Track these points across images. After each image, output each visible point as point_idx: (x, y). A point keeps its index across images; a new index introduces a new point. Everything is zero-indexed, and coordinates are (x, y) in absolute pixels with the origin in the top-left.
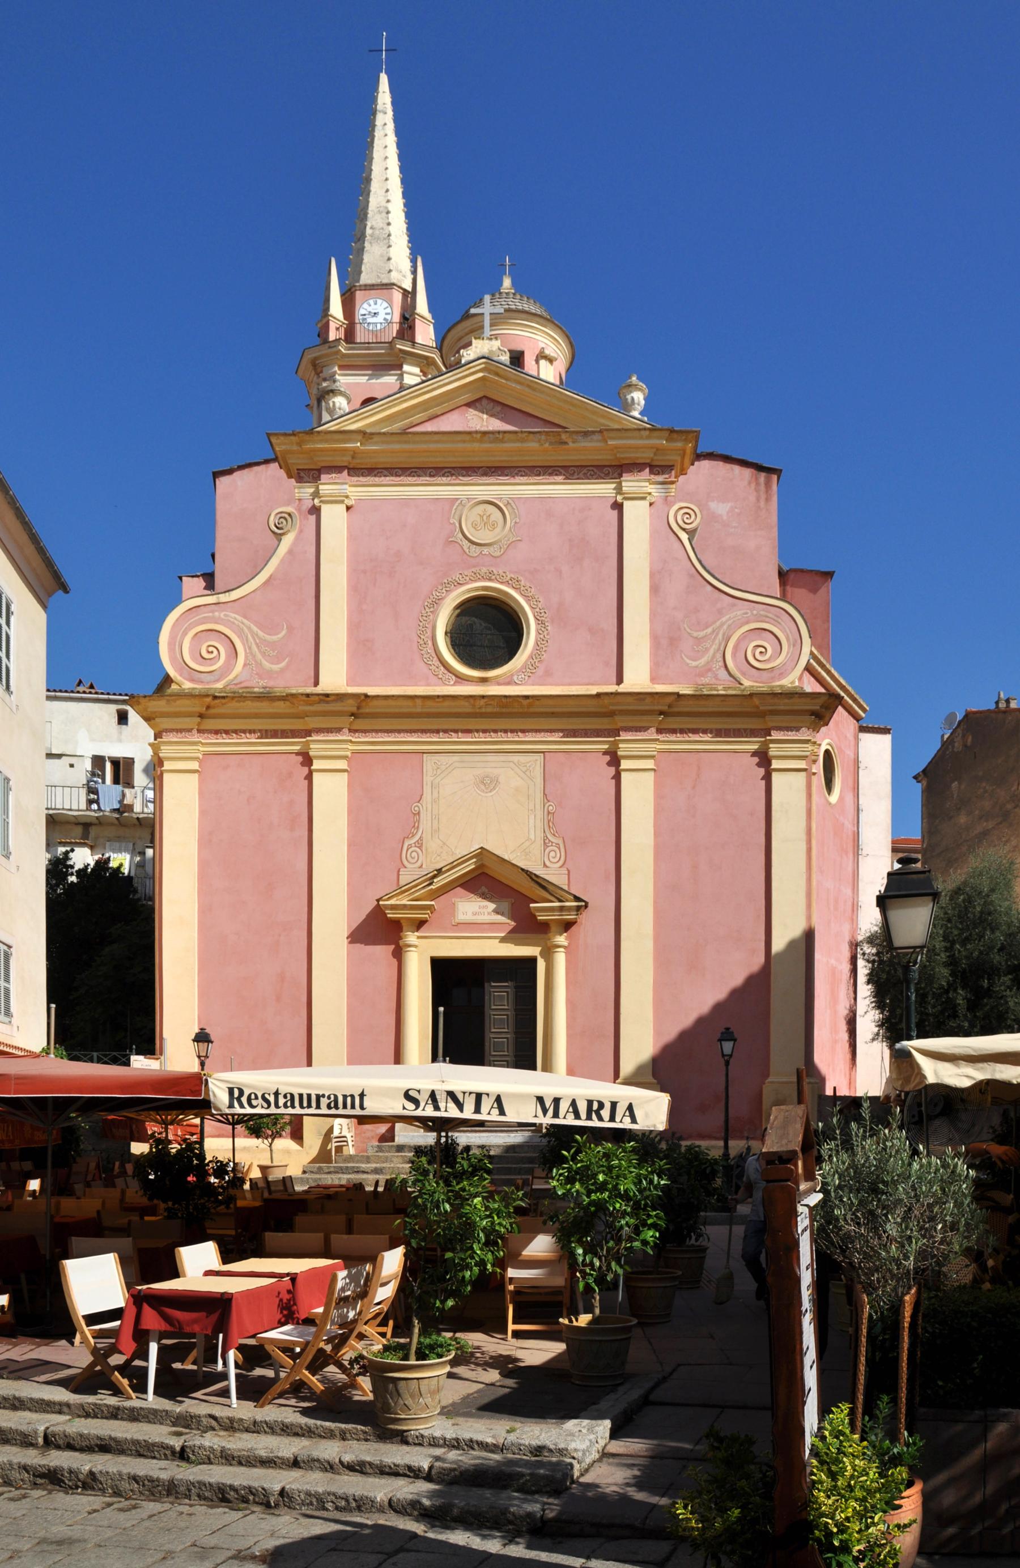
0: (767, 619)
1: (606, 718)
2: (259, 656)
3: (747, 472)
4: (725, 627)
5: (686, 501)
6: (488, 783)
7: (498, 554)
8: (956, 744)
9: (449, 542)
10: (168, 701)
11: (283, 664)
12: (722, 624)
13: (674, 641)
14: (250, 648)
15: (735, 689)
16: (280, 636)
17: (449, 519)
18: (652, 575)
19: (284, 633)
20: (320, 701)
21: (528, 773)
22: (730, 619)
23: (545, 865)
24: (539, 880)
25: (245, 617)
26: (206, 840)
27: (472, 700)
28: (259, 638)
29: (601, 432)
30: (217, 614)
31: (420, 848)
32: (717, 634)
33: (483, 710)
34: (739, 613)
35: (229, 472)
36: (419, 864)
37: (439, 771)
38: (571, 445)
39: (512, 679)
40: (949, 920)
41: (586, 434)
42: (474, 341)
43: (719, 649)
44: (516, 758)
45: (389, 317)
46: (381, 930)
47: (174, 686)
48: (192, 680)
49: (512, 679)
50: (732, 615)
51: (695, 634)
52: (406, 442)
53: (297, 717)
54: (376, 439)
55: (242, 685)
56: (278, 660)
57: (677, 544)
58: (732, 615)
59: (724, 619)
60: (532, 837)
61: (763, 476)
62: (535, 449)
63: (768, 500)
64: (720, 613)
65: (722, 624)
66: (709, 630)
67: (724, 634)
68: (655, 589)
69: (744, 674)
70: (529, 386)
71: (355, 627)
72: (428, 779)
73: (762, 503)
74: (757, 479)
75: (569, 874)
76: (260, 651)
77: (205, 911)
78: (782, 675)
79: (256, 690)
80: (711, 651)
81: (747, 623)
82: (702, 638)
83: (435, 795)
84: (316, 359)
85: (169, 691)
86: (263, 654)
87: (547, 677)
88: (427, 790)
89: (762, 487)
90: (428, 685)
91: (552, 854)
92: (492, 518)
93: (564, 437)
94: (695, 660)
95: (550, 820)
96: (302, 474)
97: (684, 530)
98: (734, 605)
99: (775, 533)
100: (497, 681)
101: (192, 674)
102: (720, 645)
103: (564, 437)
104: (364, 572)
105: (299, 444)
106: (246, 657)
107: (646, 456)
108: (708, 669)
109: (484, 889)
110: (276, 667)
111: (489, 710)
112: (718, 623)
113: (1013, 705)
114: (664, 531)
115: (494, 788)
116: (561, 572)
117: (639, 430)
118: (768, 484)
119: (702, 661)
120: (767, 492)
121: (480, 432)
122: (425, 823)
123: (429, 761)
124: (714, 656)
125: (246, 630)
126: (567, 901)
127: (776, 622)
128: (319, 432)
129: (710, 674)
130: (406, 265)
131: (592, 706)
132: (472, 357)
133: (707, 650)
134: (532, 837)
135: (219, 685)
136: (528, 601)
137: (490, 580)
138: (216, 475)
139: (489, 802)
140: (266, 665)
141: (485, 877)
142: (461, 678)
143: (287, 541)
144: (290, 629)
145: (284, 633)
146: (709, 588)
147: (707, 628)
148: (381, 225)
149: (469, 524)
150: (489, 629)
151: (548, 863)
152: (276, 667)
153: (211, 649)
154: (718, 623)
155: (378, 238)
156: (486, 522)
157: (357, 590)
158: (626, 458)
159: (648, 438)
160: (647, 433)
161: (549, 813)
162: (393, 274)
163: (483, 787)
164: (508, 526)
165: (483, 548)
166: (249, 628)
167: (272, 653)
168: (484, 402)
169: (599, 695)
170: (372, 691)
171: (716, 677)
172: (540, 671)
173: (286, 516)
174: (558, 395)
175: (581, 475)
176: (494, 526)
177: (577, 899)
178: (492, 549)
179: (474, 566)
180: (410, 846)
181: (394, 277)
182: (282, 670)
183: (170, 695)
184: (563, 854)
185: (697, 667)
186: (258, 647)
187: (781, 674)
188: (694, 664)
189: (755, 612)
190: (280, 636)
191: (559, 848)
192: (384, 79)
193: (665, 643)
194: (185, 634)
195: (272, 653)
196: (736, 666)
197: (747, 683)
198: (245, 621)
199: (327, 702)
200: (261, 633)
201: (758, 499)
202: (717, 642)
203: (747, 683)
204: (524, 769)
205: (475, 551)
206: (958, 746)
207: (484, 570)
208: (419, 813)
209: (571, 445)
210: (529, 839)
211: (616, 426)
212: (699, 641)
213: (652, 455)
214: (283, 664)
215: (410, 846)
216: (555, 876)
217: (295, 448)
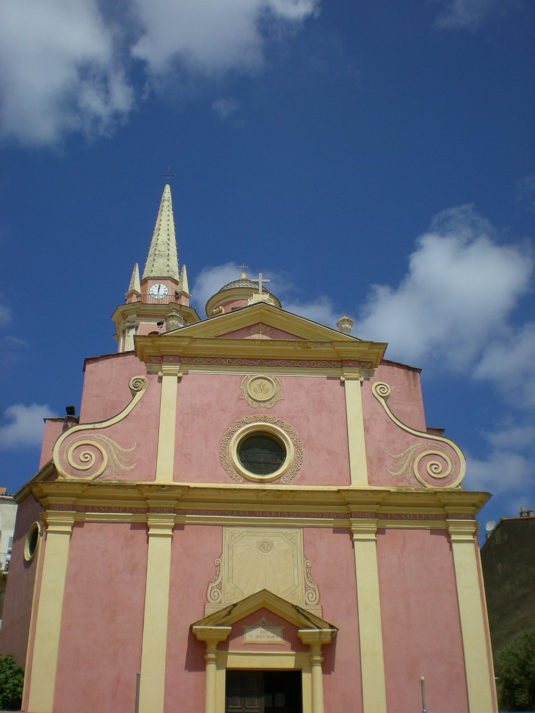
0: (437, 449)
1: (343, 511)
2: (118, 461)
3: (401, 371)
4: (412, 452)
5: (381, 381)
6: (265, 546)
7: (270, 407)
8: (497, 540)
9: (239, 399)
10: (58, 486)
11: (132, 467)
12: (410, 451)
13: (381, 460)
14: (112, 456)
15: (422, 490)
16: (132, 449)
17: (240, 386)
18: (364, 421)
19: (134, 448)
20: (159, 490)
21: (292, 540)
22: (414, 448)
23: (306, 603)
24: (305, 613)
25: (110, 437)
26: (71, 579)
27: (256, 492)
28: (118, 450)
29: (331, 342)
30: (92, 435)
31: (220, 589)
32: (407, 456)
33: (263, 499)
34: (419, 444)
35: (95, 360)
36: (219, 600)
37: (233, 538)
38: (313, 349)
39: (282, 480)
40: (503, 656)
41: (322, 343)
42: (254, 294)
43: (409, 466)
44: (284, 530)
45: (166, 293)
46: (198, 651)
47: (60, 478)
48: (72, 474)
49: (282, 480)
50: (415, 446)
51: (394, 456)
52: (216, 344)
53: (142, 504)
54: (198, 341)
55: (105, 479)
56: (130, 463)
57: (379, 405)
58: (415, 446)
59: (410, 448)
60: (296, 583)
61: (411, 373)
62: (291, 350)
63: (415, 385)
64: (408, 444)
65: (410, 451)
66: (402, 454)
67: (411, 456)
68: (367, 430)
69: (426, 481)
70: (287, 318)
71: (179, 446)
72: (226, 542)
73: (412, 387)
74: (408, 374)
75: (322, 609)
76: (118, 458)
77: (66, 628)
78: (450, 482)
79: (113, 482)
80: (405, 467)
81: (425, 450)
82: (398, 459)
83: (231, 553)
84: (124, 311)
85: (57, 480)
86: (120, 460)
87: (302, 480)
88: (225, 550)
89: (412, 378)
90: (226, 483)
91: (310, 595)
92: (266, 387)
93: (309, 344)
94: (395, 472)
95: (309, 573)
96: (152, 358)
97: (382, 397)
98: (416, 440)
99: (421, 403)
100: (270, 481)
101: (73, 471)
102: (409, 463)
103: (309, 344)
104: (188, 414)
105: (153, 342)
106: (108, 462)
107: (356, 356)
108: (402, 478)
109: (264, 619)
110: (128, 468)
111: (267, 499)
112: (407, 450)
113: (532, 515)
114: (368, 399)
115: (270, 550)
116: (308, 418)
117: (353, 342)
118: (414, 377)
119: (399, 473)
120: (414, 381)
121: (260, 340)
122: (224, 572)
123: (227, 531)
124: (406, 470)
125: (110, 446)
126: (324, 628)
127: (443, 451)
128: (165, 336)
129: (405, 481)
130: (176, 269)
131: (334, 499)
132: (252, 303)
133: (402, 466)
134: (296, 583)
135: (90, 478)
136: (289, 435)
137: (265, 421)
138: (87, 361)
139: (263, 562)
140: (122, 467)
141: (263, 611)
142: (248, 480)
143: (139, 395)
144: (138, 445)
145: (134, 448)
146: (399, 429)
147: (400, 452)
148: (164, 250)
149: (252, 390)
150: (262, 449)
151: (308, 602)
152: (128, 468)
153: (86, 456)
154: (407, 450)
155: (162, 256)
156: (262, 388)
157: (181, 424)
158: (346, 357)
159: (358, 346)
160: (358, 344)
161: (307, 567)
162: (170, 273)
163: (263, 549)
164: (270, 396)
165: (260, 403)
166: (112, 445)
167: (126, 460)
168: (260, 325)
169: (339, 491)
170: (192, 485)
171: (409, 482)
172: (298, 477)
173: (141, 381)
174: (304, 323)
175: (318, 365)
176: (267, 391)
177: (331, 627)
178: (266, 403)
179: (255, 413)
180: (213, 588)
181: (171, 274)
182: (132, 470)
183: (57, 482)
184: (318, 595)
185: (397, 476)
186: (117, 455)
187: (449, 481)
188: (394, 474)
189: (429, 444)
190: (132, 449)
191: (315, 591)
192: (168, 188)
193: (375, 461)
194: (71, 445)
195: (126, 460)
196: (421, 475)
197: (429, 486)
198: (110, 440)
199: (163, 491)
200: (119, 447)
201: (410, 384)
202: (408, 461)
203: (427, 485)
204: (290, 538)
205: (256, 405)
206: (498, 540)
207: (261, 415)
208: (219, 565)
209: (313, 349)
210: (294, 585)
211: (339, 340)
212: (396, 460)
213: (360, 356)
214: (132, 467)
215: (213, 588)
216: (314, 610)
217: (150, 344)
